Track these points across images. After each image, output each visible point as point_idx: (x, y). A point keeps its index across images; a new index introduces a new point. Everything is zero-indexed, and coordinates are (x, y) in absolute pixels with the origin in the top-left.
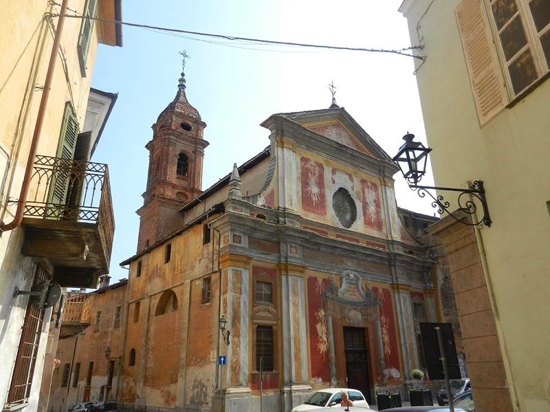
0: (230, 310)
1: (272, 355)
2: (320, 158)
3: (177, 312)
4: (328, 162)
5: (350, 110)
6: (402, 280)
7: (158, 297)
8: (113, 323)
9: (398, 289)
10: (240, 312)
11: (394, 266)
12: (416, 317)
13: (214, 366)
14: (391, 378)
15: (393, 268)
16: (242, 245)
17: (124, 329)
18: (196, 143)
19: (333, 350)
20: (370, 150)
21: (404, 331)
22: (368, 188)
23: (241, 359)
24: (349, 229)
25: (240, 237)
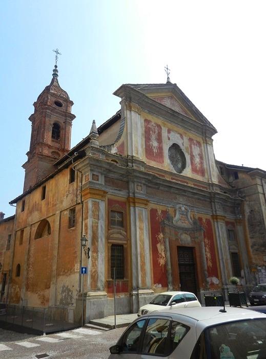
0: (90, 232)
1: (123, 267)
2: (159, 121)
3: (50, 236)
4: (165, 124)
5: (181, 86)
6: (220, 213)
7: (37, 225)
8: (6, 246)
9: (217, 219)
10: (98, 234)
11: (214, 202)
12: (230, 240)
13: (78, 275)
14: (212, 284)
15: (213, 204)
16: (99, 183)
17: (13, 250)
18: (66, 116)
19: (169, 263)
20: (195, 117)
21: (221, 250)
22: (194, 145)
23: (99, 270)
24: (181, 174)
25: (98, 176)
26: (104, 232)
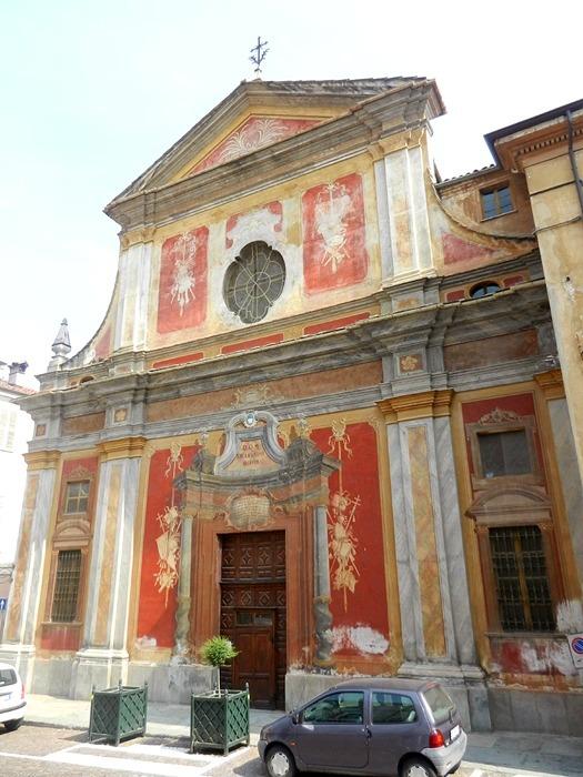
19: (187, 584)
26: (44, 529)
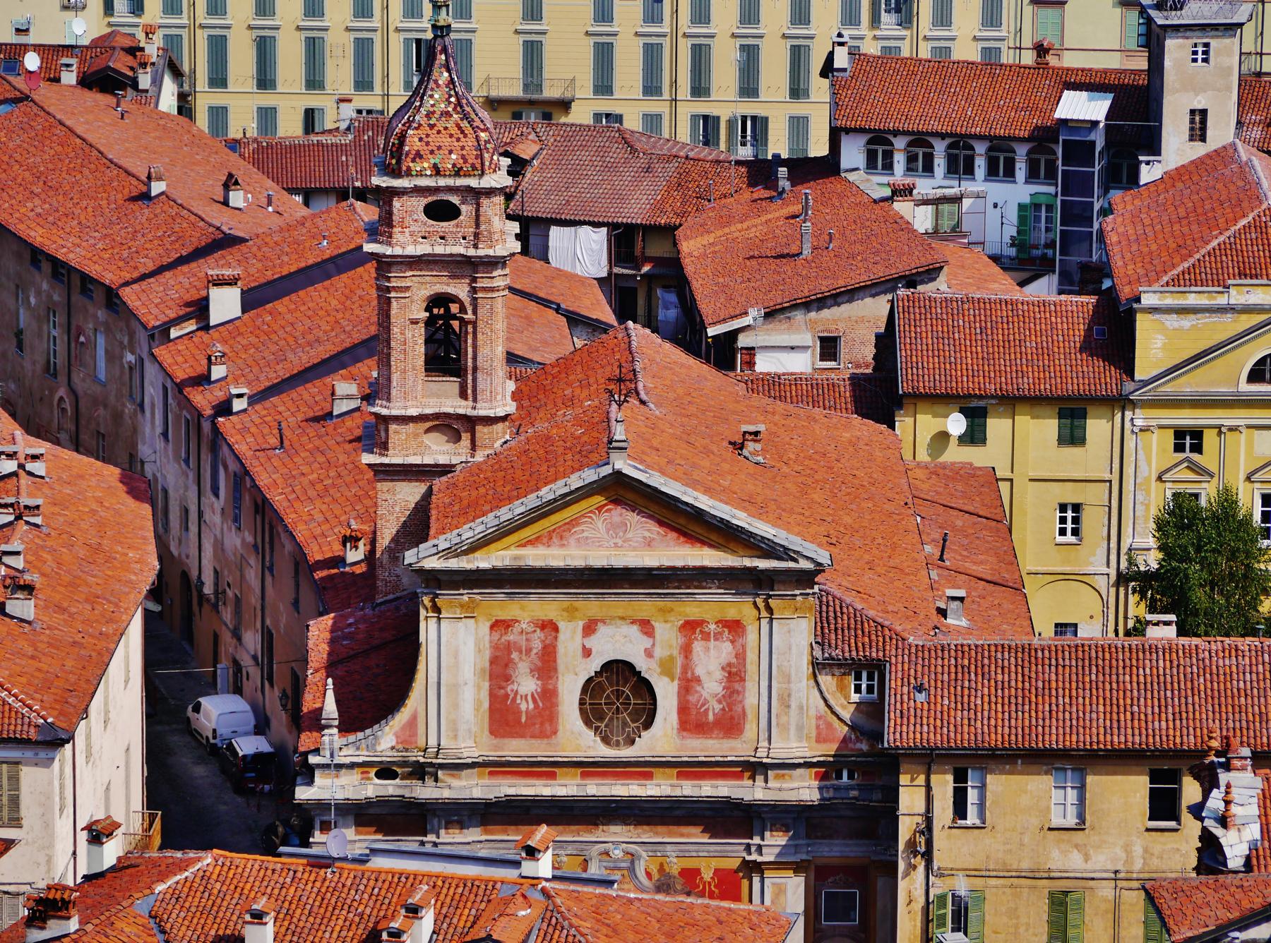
16: (969, 822)
